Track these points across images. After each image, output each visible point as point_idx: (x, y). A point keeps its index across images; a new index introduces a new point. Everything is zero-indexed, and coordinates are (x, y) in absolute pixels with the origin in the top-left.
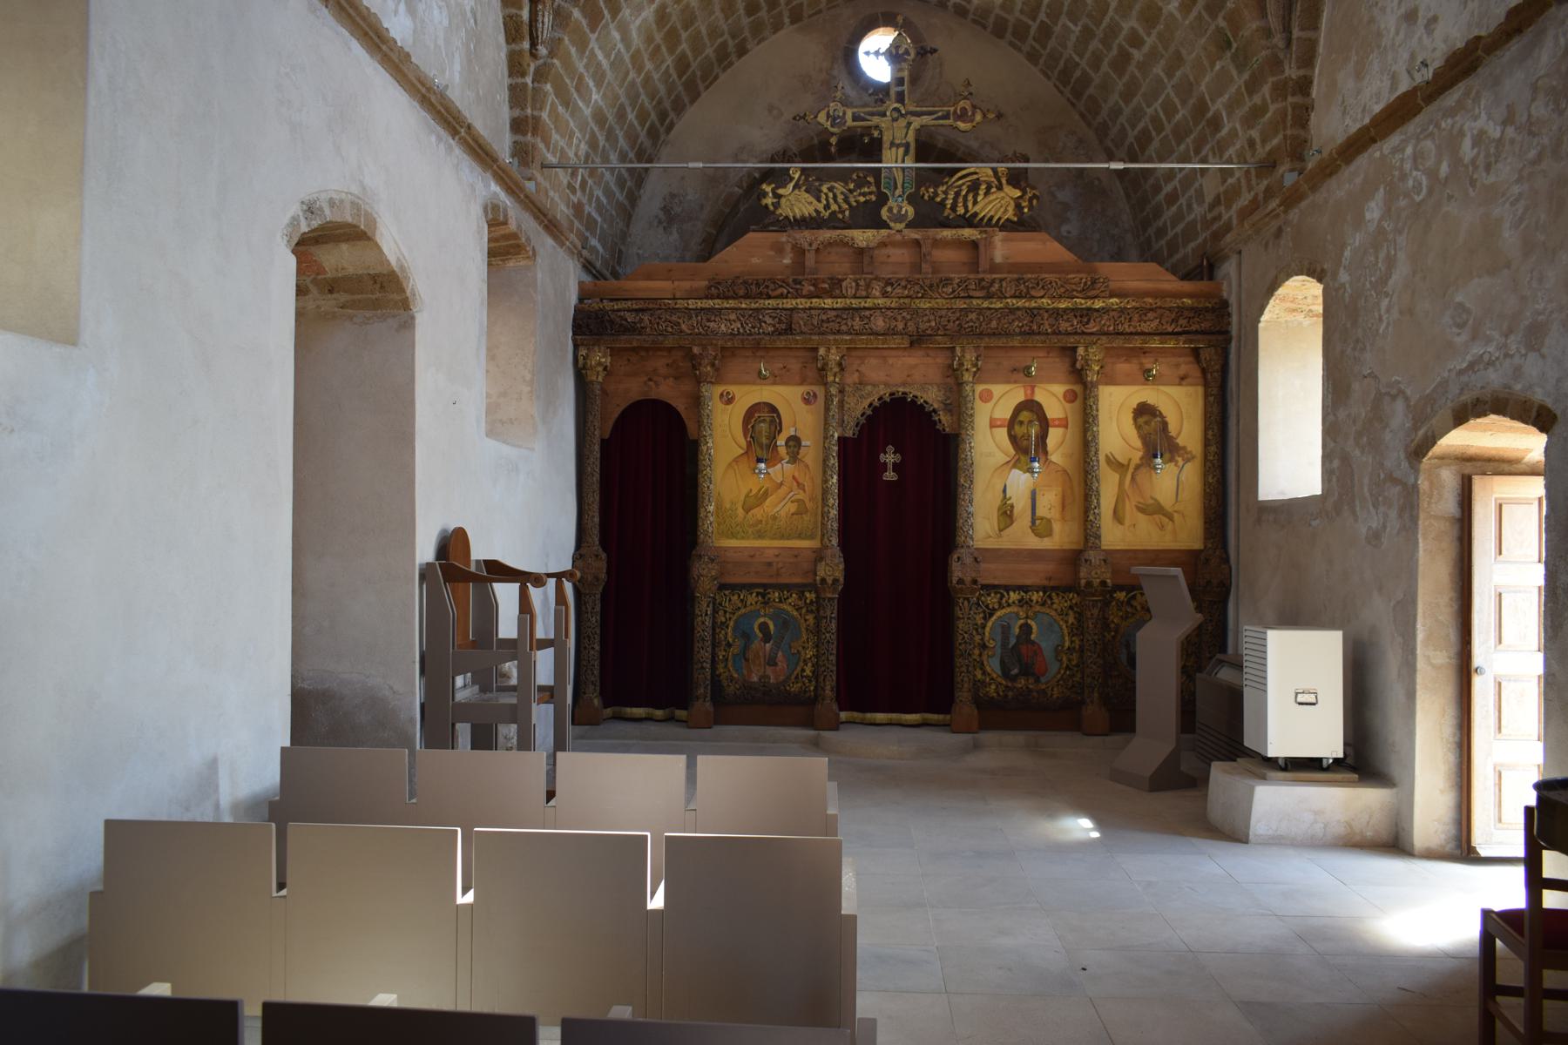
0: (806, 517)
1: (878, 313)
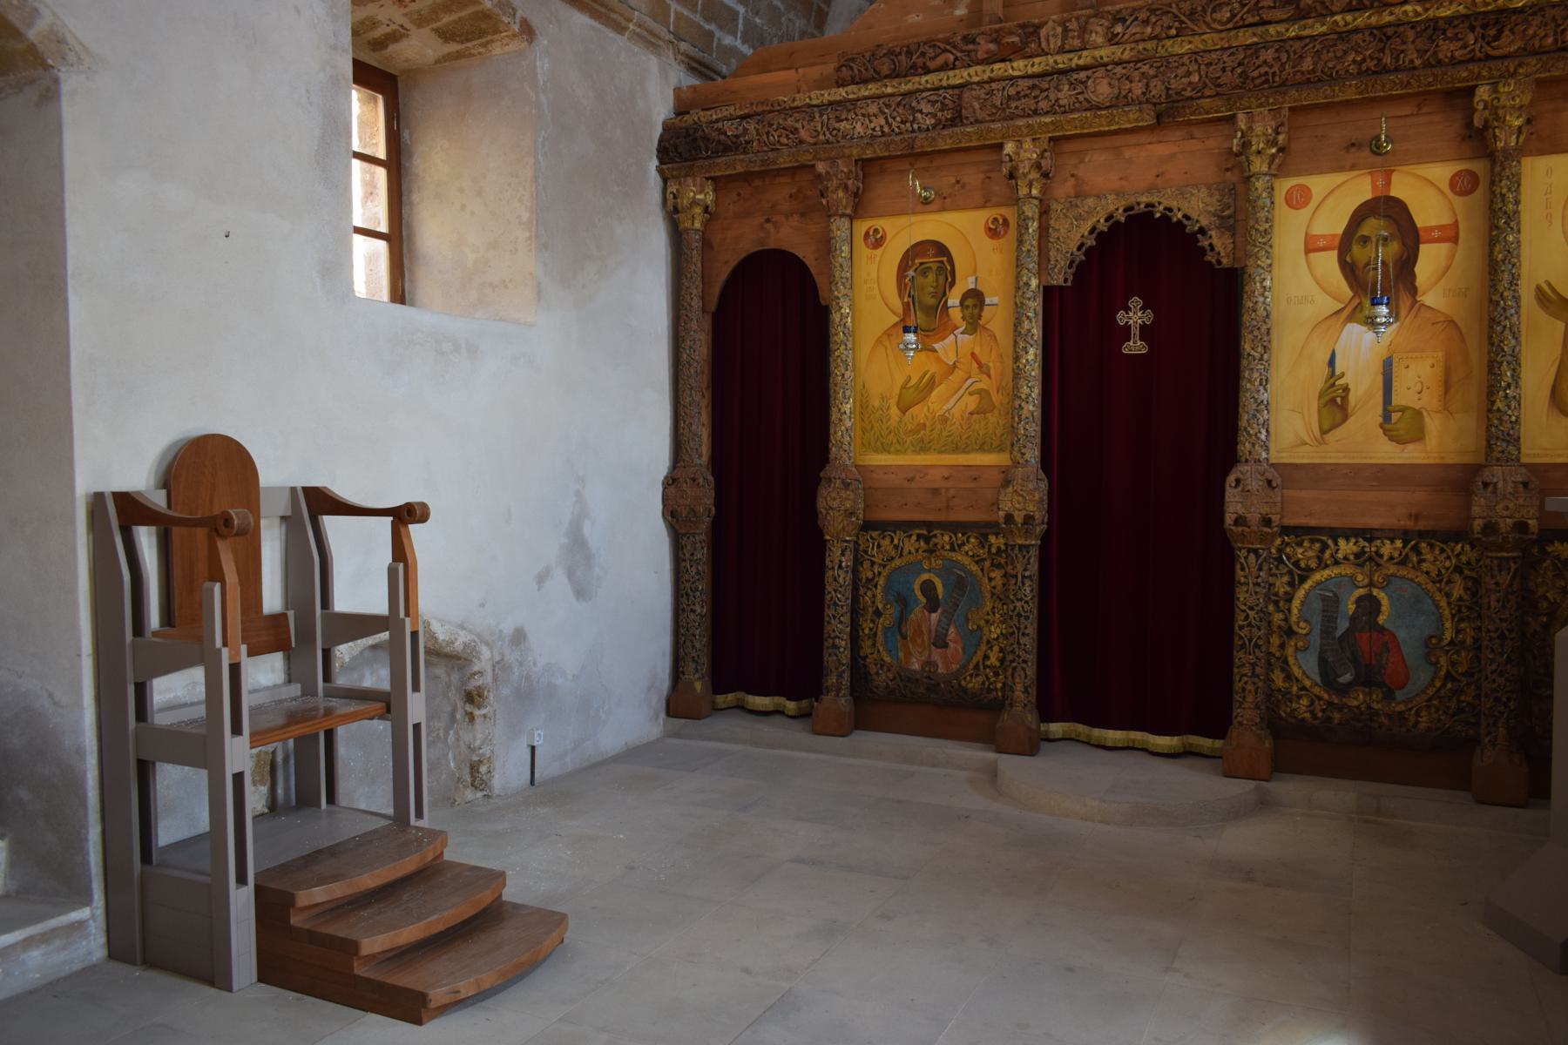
0: (992, 418)
1: (1101, 72)
